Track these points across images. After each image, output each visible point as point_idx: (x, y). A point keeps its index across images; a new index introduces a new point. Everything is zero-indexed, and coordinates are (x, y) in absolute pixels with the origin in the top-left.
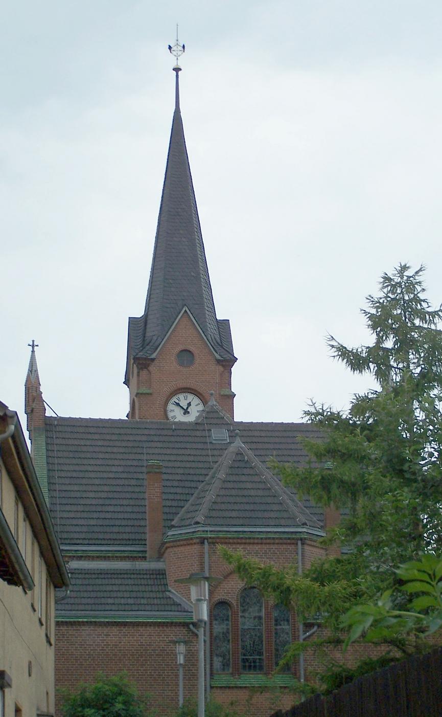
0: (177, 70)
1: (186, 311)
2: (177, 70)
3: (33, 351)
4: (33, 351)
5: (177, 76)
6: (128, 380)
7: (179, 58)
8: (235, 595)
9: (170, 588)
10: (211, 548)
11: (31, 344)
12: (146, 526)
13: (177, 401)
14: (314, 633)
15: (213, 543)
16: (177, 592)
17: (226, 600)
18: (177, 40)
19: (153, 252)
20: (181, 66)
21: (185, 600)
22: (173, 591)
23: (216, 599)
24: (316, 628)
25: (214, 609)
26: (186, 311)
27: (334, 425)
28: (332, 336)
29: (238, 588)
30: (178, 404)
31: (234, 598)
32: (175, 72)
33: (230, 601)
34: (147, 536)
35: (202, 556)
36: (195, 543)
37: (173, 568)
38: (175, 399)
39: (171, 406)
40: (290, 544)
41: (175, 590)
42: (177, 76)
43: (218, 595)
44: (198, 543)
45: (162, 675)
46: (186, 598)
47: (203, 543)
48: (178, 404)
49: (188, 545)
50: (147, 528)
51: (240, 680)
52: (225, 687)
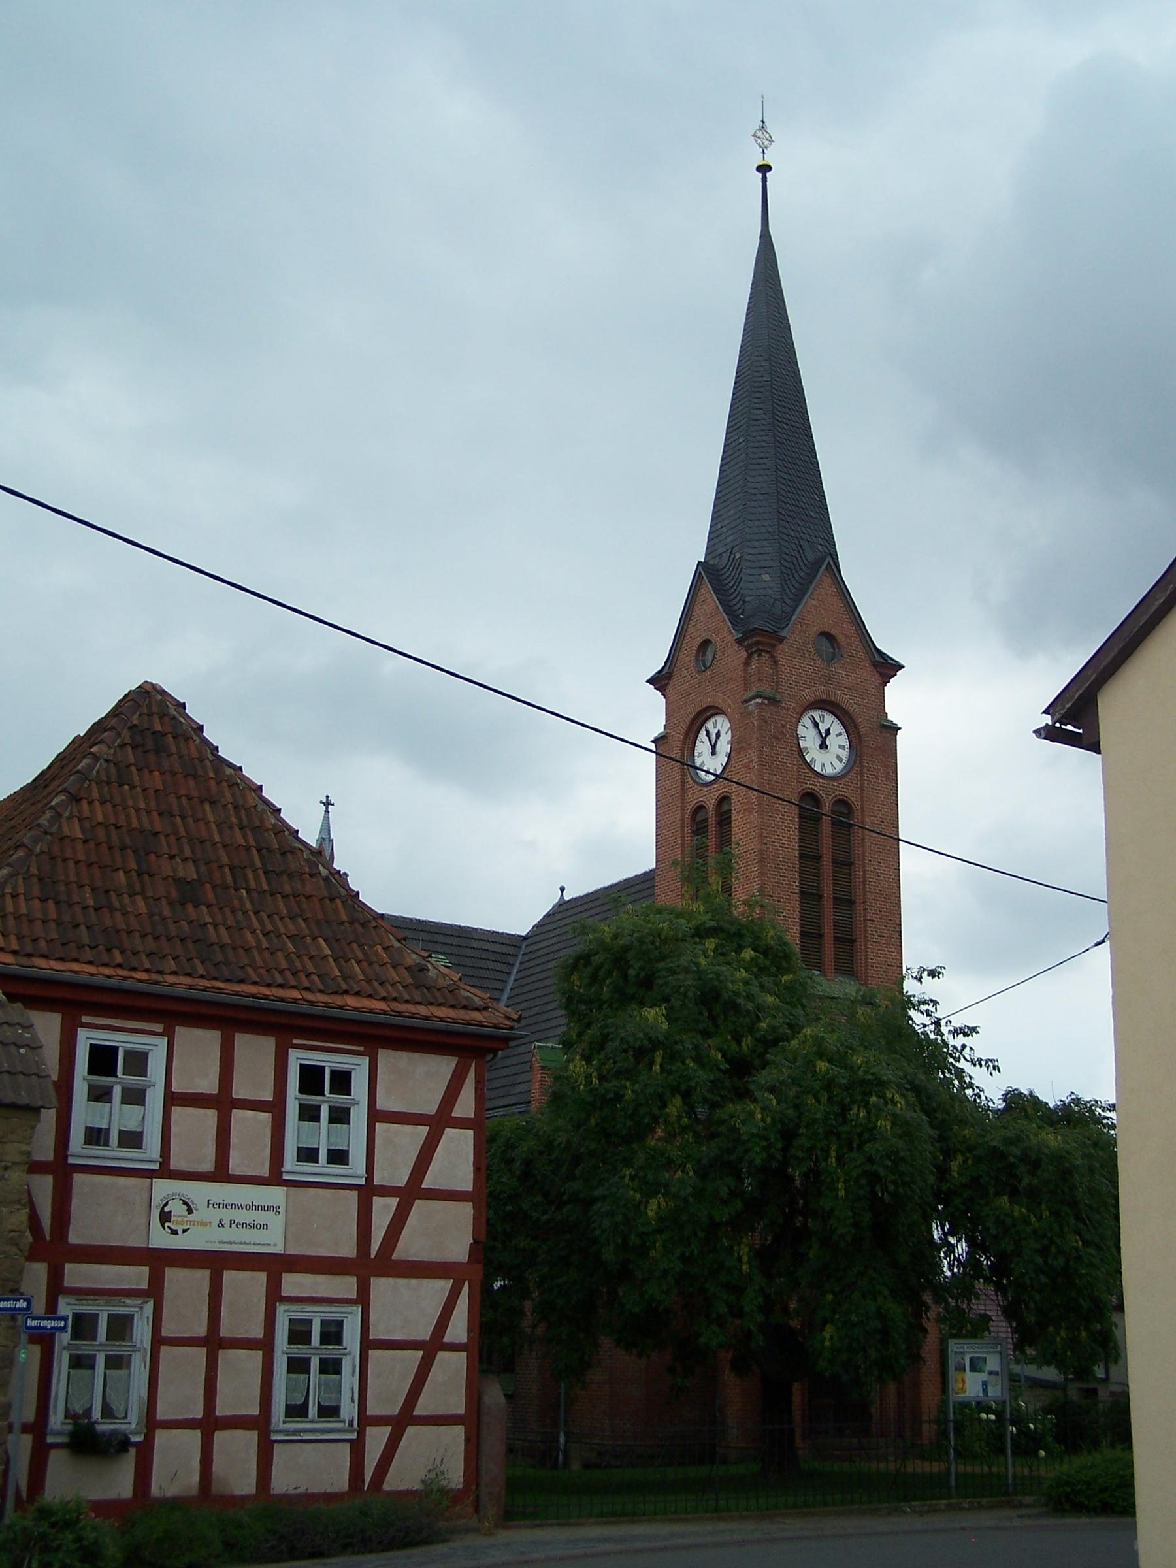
0: (764, 169)
1: (829, 563)
2: (764, 169)
3: (327, 811)
4: (327, 811)
5: (764, 180)
6: (669, 676)
7: (765, 151)
11: (325, 800)
13: (818, 720)
18: (763, 122)
19: (631, 874)
20: (768, 161)
26: (829, 563)
28: (189, 1231)
30: (816, 725)
32: (760, 175)
38: (816, 714)
39: (806, 720)
42: (764, 180)
48: (816, 725)
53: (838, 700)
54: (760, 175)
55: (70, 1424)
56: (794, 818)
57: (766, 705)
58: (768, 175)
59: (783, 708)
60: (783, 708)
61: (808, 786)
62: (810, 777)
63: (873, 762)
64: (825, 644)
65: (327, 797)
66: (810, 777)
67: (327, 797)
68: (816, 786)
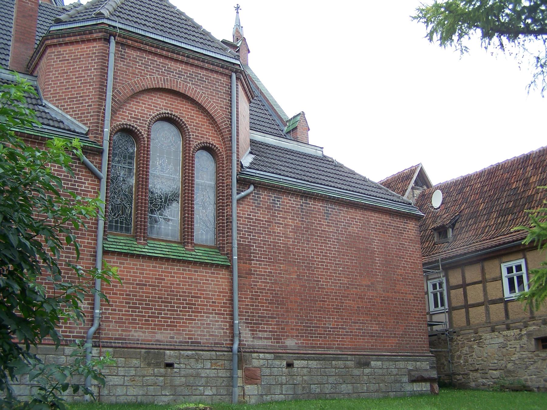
8: (145, 124)
9: (45, 102)
10: (119, 51)
12: (8, 60)
14: (248, 195)
15: (122, 44)
16: (57, 107)
17: (133, 127)
21: (69, 117)
22: (50, 105)
23: (118, 123)
24: (252, 188)
25: (116, 133)
27: (32, 308)
29: (150, 115)
31: (145, 127)
33: (138, 130)
34: (11, 48)
35: (105, 57)
36: (95, 40)
37: (53, 74)
40: (221, 74)
41: (54, 104)
43: (122, 118)
44: (100, 39)
45: (59, 74)
46: (71, 115)
47: (108, 41)
49: (83, 41)
50: (11, 47)
51: (147, 247)
52: (126, 254)
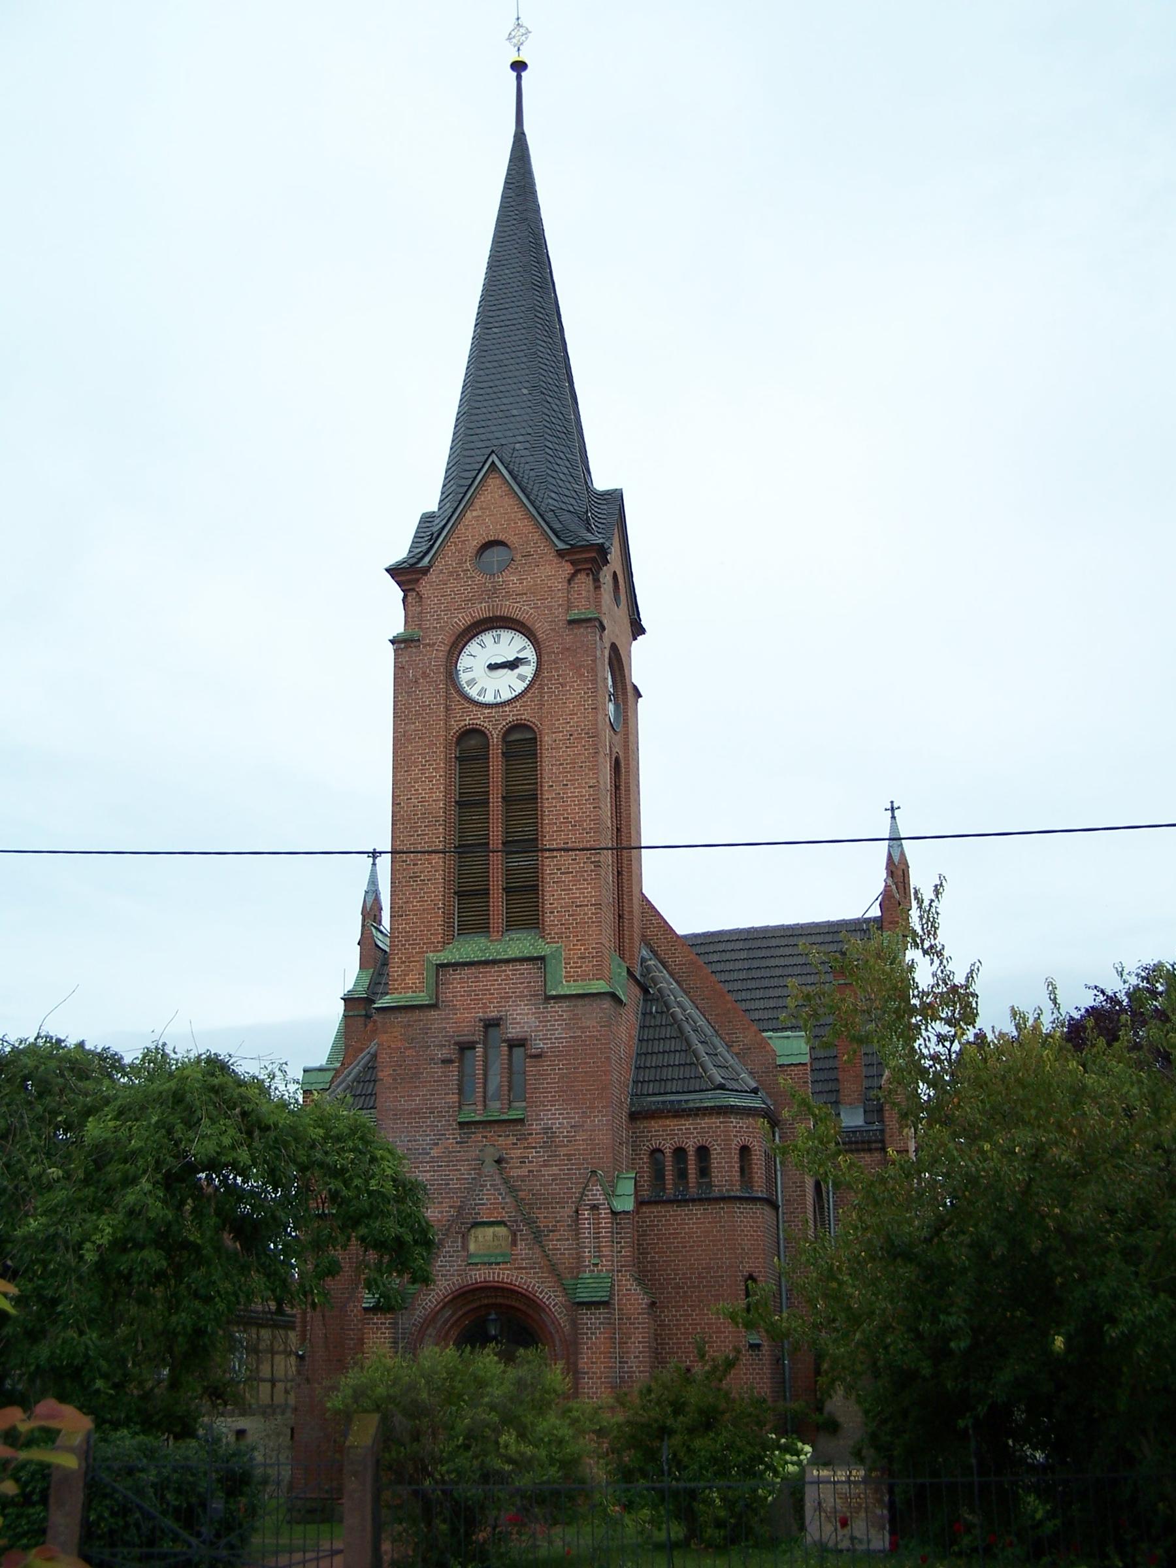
0: (519, 67)
2: (519, 67)
3: (893, 817)
4: (893, 817)
5: (519, 78)
42: (519, 78)
53: (505, 612)
54: (514, 74)
55: (286, 1371)
56: (439, 764)
57: (402, 649)
58: (523, 74)
59: (426, 645)
60: (426, 645)
61: (467, 723)
62: (472, 711)
63: (557, 669)
64: (495, 555)
65: (899, 808)
66: (472, 711)
67: (899, 808)
68: (479, 719)
